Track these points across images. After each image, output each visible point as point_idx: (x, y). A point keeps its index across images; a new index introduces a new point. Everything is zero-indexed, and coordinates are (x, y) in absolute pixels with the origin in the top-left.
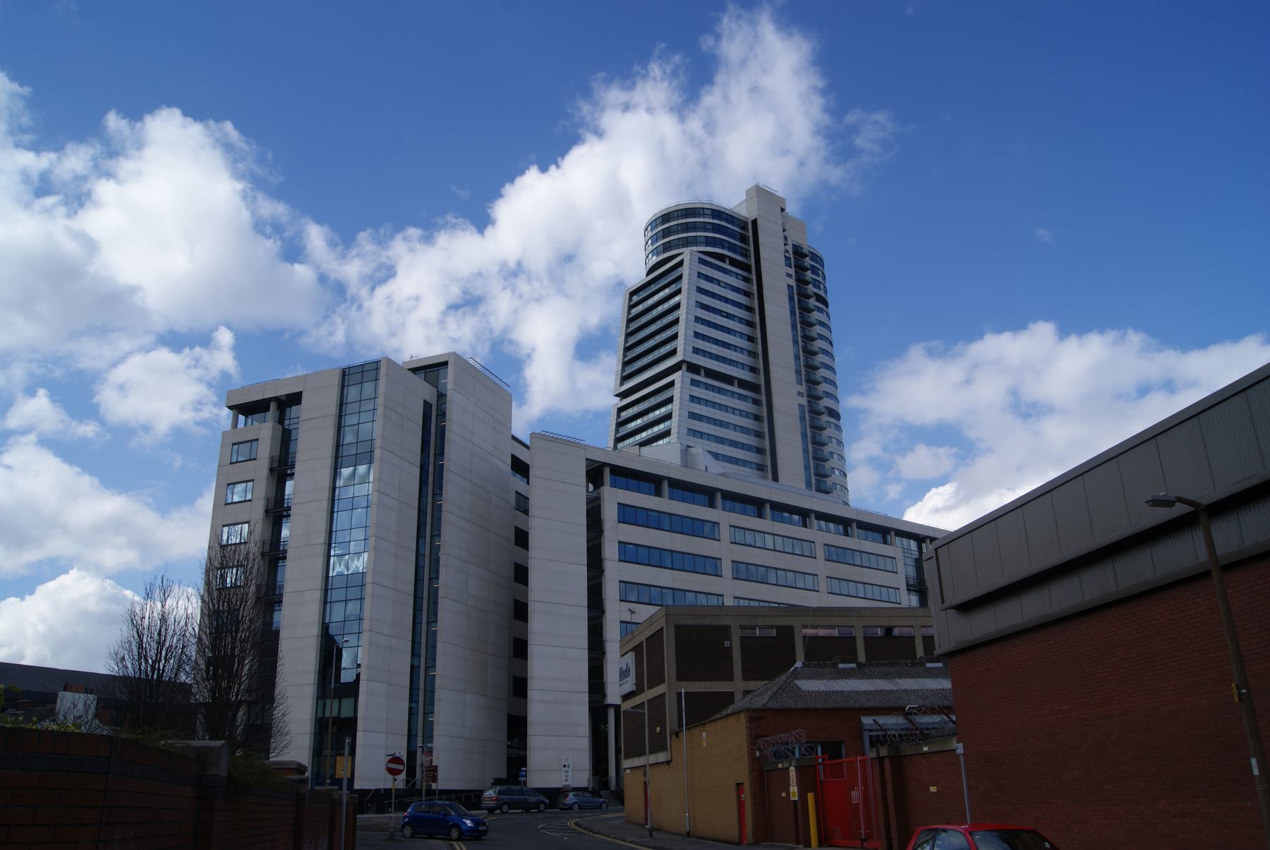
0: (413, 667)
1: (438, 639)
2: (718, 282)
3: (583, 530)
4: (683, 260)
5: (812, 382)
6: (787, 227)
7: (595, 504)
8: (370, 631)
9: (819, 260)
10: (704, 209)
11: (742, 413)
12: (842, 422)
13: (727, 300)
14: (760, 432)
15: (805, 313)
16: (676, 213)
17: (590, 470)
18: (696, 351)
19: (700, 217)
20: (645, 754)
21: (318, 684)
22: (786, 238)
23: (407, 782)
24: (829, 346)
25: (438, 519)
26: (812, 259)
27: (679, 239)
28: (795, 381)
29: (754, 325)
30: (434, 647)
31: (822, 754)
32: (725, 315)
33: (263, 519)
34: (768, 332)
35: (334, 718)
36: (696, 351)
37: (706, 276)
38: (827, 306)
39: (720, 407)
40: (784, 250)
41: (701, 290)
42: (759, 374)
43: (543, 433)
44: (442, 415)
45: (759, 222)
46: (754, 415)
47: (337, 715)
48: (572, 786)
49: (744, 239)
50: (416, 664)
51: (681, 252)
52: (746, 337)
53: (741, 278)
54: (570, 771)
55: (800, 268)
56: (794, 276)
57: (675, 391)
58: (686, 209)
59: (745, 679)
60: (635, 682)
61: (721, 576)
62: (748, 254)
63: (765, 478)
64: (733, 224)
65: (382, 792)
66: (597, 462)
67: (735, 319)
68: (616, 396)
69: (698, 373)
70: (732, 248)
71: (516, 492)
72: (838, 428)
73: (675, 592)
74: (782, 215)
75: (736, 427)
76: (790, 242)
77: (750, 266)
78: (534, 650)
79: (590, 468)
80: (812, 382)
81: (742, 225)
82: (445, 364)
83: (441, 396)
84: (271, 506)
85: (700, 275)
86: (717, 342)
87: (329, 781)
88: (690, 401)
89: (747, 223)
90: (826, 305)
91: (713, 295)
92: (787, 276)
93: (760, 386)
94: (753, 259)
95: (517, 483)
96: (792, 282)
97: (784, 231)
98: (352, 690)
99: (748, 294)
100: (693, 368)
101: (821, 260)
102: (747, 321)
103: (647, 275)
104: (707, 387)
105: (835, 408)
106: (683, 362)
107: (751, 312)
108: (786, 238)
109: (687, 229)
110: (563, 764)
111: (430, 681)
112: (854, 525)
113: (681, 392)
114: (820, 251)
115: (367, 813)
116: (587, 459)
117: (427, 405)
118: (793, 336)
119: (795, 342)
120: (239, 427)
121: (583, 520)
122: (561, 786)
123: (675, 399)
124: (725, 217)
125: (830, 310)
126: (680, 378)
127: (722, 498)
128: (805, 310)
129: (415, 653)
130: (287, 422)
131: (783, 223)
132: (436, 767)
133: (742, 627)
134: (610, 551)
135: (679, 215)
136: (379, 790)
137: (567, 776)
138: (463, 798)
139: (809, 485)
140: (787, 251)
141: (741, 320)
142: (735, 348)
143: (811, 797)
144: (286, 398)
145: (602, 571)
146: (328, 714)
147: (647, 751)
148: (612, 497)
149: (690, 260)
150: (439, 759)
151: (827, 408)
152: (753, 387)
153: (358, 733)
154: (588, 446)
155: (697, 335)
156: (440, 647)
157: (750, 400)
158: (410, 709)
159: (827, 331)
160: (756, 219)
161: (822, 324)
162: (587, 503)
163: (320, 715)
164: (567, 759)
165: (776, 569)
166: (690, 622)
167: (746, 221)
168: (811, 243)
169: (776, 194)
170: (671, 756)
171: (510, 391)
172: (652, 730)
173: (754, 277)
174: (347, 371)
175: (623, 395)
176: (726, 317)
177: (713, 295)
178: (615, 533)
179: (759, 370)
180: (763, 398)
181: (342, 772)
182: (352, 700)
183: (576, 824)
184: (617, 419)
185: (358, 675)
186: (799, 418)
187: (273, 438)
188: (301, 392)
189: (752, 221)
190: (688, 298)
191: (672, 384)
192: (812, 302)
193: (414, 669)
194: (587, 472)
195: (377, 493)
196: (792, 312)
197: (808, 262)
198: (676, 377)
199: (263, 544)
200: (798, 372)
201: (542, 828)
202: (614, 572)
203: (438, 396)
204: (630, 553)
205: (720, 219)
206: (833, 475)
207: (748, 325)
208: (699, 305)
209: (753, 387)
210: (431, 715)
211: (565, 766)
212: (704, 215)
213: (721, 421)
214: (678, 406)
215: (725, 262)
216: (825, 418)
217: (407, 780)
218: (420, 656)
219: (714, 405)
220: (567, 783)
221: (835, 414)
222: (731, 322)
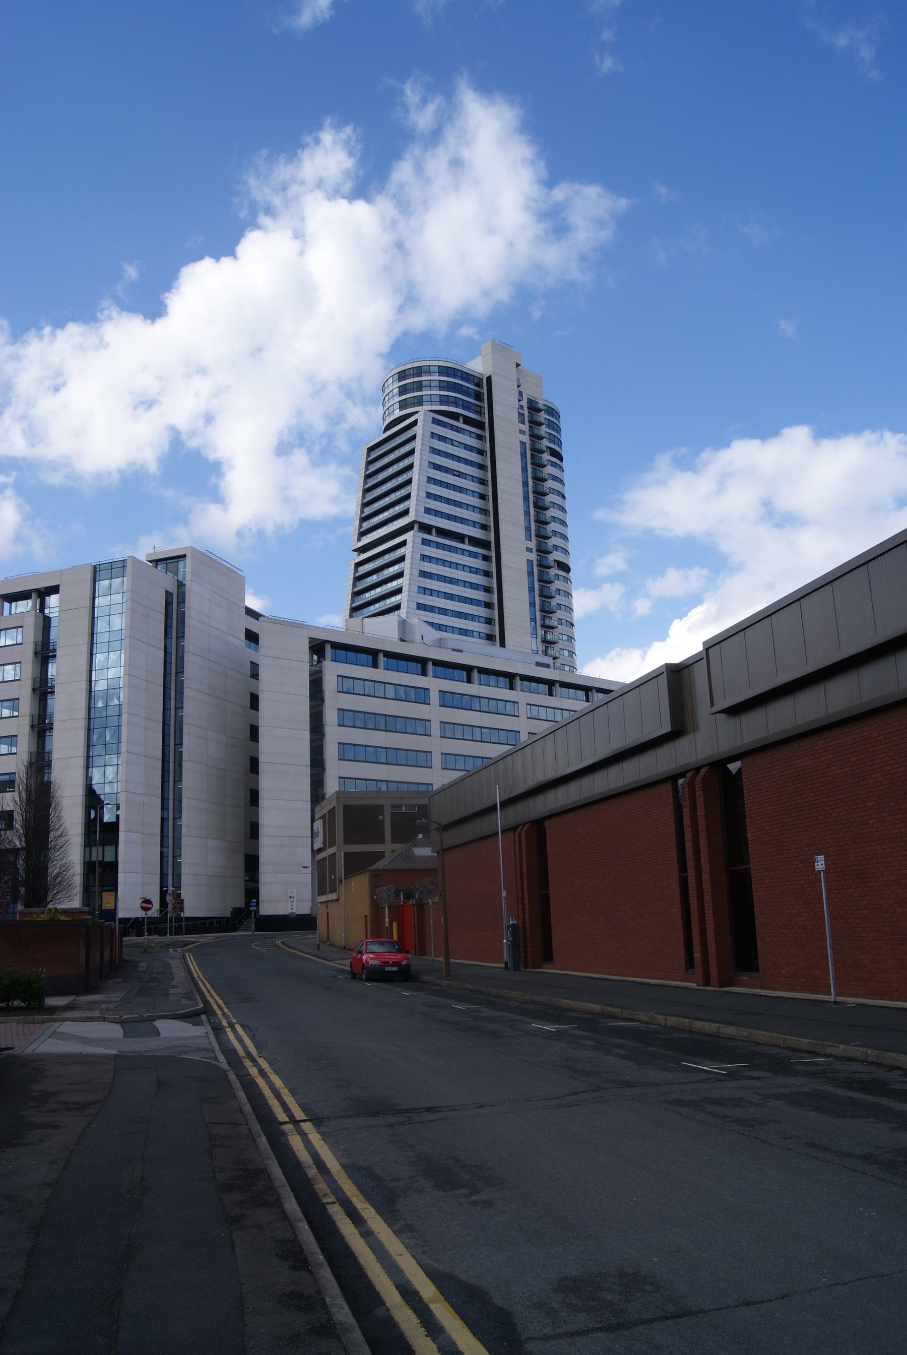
0: (163, 819)
1: (183, 795)
2: (452, 442)
3: (307, 700)
4: (417, 420)
5: (542, 537)
6: (522, 381)
7: (318, 676)
8: (126, 791)
11: (472, 569)
12: (571, 575)
13: (459, 459)
14: (489, 587)
18: (428, 511)
20: (327, 893)
21: (85, 835)
22: (521, 394)
23: (161, 912)
25: (181, 692)
28: (524, 538)
29: (486, 482)
30: (181, 801)
31: (404, 899)
32: (457, 473)
33: (31, 696)
34: (498, 490)
35: (99, 861)
36: (428, 511)
38: (561, 460)
39: (451, 564)
40: (517, 406)
41: (434, 451)
43: (270, 617)
44: (182, 601)
47: (101, 859)
48: (296, 913)
49: (478, 396)
50: (165, 816)
51: (416, 411)
53: (474, 435)
54: (295, 902)
55: (534, 423)
59: (393, 842)
60: (322, 841)
61: (430, 736)
62: (482, 412)
64: (467, 381)
65: (140, 920)
66: (317, 640)
68: (354, 551)
69: (430, 533)
70: (466, 406)
71: (251, 662)
72: (567, 580)
73: (388, 750)
74: (517, 369)
77: (484, 424)
78: (264, 802)
80: (542, 537)
82: (184, 556)
83: (181, 585)
84: (37, 686)
85: (433, 435)
86: (448, 501)
87: (98, 912)
91: (446, 455)
92: (520, 432)
93: (490, 542)
94: (487, 416)
95: (249, 654)
96: (526, 439)
97: (518, 386)
98: (113, 828)
99: (481, 452)
100: (426, 528)
103: (385, 431)
104: (438, 545)
105: (564, 561)
106: (414, 522)
107: (482, 440)
108: (521, 394)
110: (289, 896)
111: (177, 830)
112: (558, 685)
113: (413, 552)
114: (557, 405)
115: (128, 936)
117: (168, 594)
120: (4, 615)
121: (306, 692)
122: (288, 914)
124: (460, 375)
125: (564, 464)
126: (412, 538)
127: (433, 665)
128: (538, 465)
129: (164, 807)
130: (47, 611)
131: (518, 379)
132: (183, 900)
133: (393, 807)
134: (330, 717)
136: (138, 918)
137: (292, 905)
138: (215, 922)
140: (521, 407)
142: (467, 506)
143: (395, 924)
144: (45, 590)
145: (323, 735)
146: (94, 859)
147: (328, 892)
148: (332, 670)
150: (186, 893)
152: (485, 544)
153: (119, 874)
154: (310, 626)
155: (429, 495)
156: (185, 802)
157: (480, 557)
158: (162, 853)
160: (491, 376)
162: (310, 675)
163: (87, 859)
164: (292, 892)
165: (481, 727)
166: (354, 803)
168: (546, 396)
170: (339, 896)
171: (243, 575)
172: (330, 877)
173: (487, 435)
174: (98, 567)
175: (362, 550)
176: (459, 476)
177: (446, 455)
178: (333, 702)
180: (493, 554)
181: (108, 904)
182: (113, 847)
183: (282, 943)
184: (354, 574)
185: (118, 817)
186: (527, 573)
187: (36, 625)
188: (59, 586)
189: (487, 378)
191: (403, 544)
192: (546, 457)
193: (163, 820)
195: (127, 676)
196: (524, 469)
197: (543, 416)
198: (408, 536)
199: (33, 717)
201: (254, 945)
202: (334, 735)
203: (178, 586)
204: (347, 718)
205: (455, 376)
207: (481, 483)
208: (432, 465)
209: (485, 544)
210: (179, 857)
211: (290, 897)
213: (451, 578)
215: (458, 421)
216: (554, 571)
217: (160, 910)
218: (168, 810)
219: (444, 562)
220: (292, 911)
221: (565, 568)
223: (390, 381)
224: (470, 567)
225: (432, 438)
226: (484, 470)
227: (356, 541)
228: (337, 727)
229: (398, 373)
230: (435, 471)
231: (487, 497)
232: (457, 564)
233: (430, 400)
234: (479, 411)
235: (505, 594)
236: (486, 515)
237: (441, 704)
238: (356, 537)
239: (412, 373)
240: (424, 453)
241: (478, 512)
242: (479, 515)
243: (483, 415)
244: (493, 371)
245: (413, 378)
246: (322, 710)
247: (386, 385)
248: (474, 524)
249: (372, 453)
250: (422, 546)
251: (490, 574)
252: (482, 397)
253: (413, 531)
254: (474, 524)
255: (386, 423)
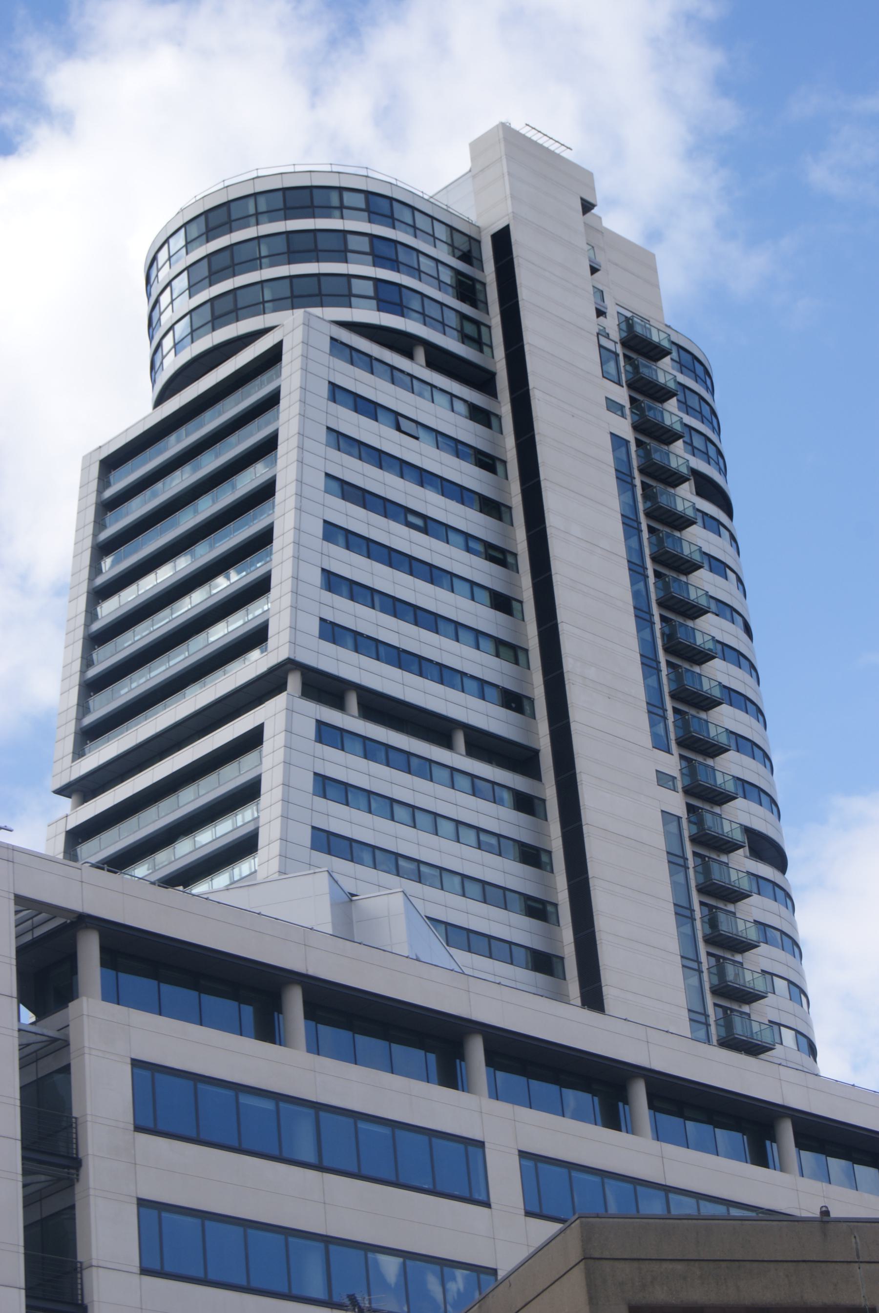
2: (397, 420)
7: (49, 1065)
9: (699, 370)
10: (341, 190)
11: (484, 837)
12: (793, 877)
15: (686, 665)
16: (251, 202)
17: (35, 942)
19: (329, 216)
24: (744, 637)
26: (682, 367)
27: (258, 238)
29: (510, 559)
37: (356, 396)
38: (730, 513)
42: (533, 717)
45: (516, 236)
46: (527, 898)
51: (268, 325)
52: (485, 596)
56: (627, 411)
57: (267, 762)
58: (284, 190)
62: (485, 339)
63: (560, 996)
66: (54, 910)
67: (452, 536)
69: (339, 704)
75: (442, 439)
76: (612, 310)
79: (28, 938)
81: (465, 247)
85: (336, 392)
88: (328, 399)
89: (479, 242)
90: (727, 506)
94: (500, 352)
97: (594, 270)
101: (707, 373)
102: (488, 545)
106: (289, 665)
107: (489, 425)
108: (600, 294)
109: (293, 296)
116: (21, 901)
118: (636, 595)
119: (642, 616)
123: (262, 841)
125: (738, 524)
135: (263, 207)
139: (698, 1018)
140: (602, 333)
141: (468, 540)
149: (306, 343)
151: (748, 831)
159: (754, 721)
161: (719, 567)
162: (24, 1063)
167: (474, 234)
169: (566, 154)
176: (425, 531)
179: (531, 701)
180: (549, 791)
190: (301, 462)
194: (22, 951)
198: (276, 706)
200: (655, 710)
206: (777, 1046)
212: (341, 209)
213: (419, 862)
214: (277, 809)
222: (443, 594)
223: (178, 241)
224: (479, 830)
225: (335, 401)
226: (500, 519)
227: (70, 756)
228: (137, 1278)
229: (187, 268)
230: (349, 505)
231: (515, 605)
232: (436, 815)
233: (317, 292)
234: (476, 336)
235: (603, 924)
236: (517, 663)
237: (529, 1209)
238: (69, 744)
239: (252, 211)
240: (308, 444)
241: (493, 651)
242: (494, 661)
243: (486, 349)
244: (513, 212)
245: (257, 224)
246: (73, 1207)
247: (163, 256)
248: (482, 687)
249: (114, 475)
250: (319, 745)
251: (544, 858)
252: (481, 297)
253: (285, 693)
254: (482, 687)
255: (163, 378)
